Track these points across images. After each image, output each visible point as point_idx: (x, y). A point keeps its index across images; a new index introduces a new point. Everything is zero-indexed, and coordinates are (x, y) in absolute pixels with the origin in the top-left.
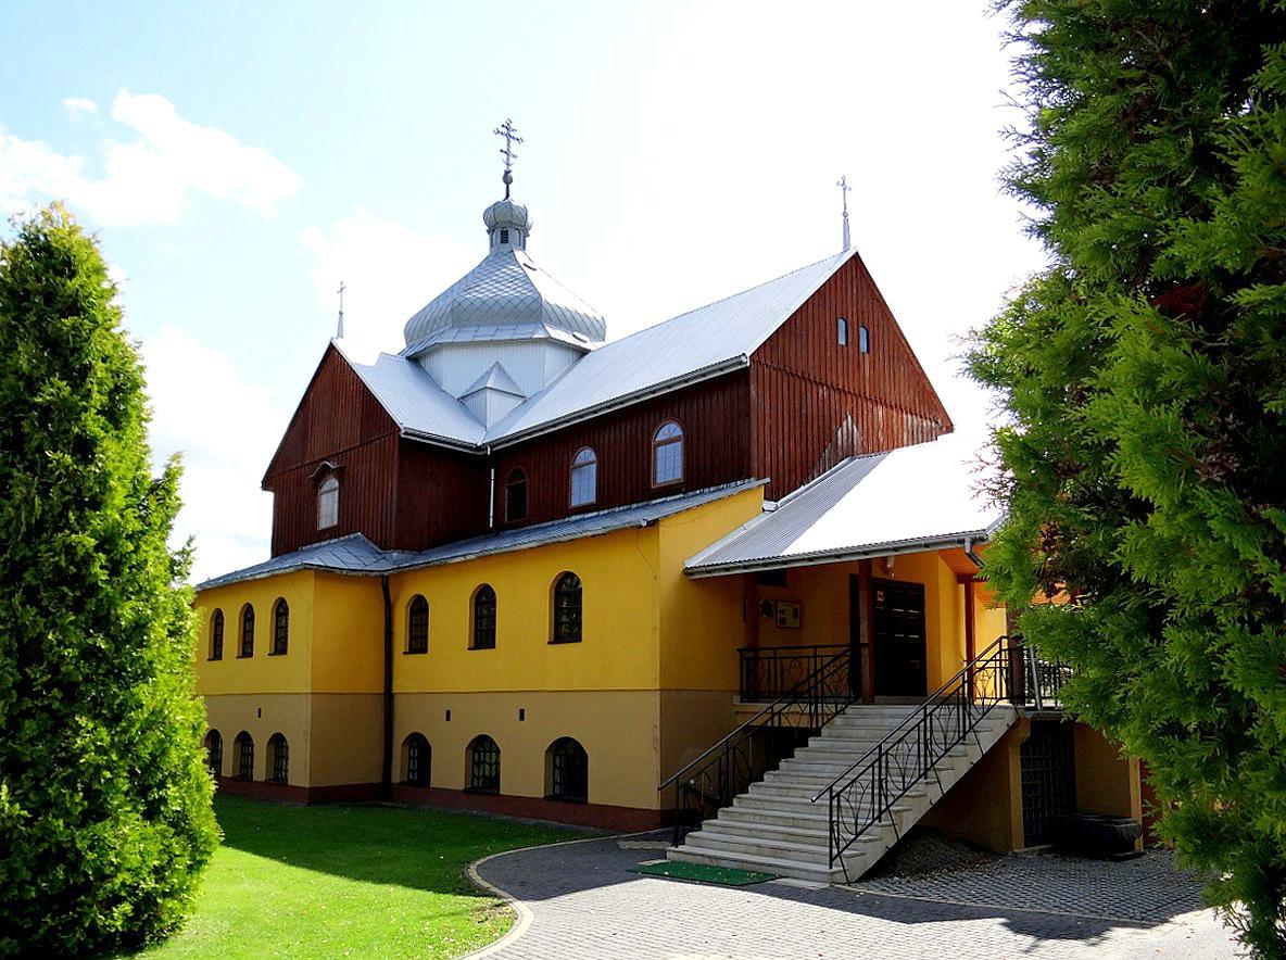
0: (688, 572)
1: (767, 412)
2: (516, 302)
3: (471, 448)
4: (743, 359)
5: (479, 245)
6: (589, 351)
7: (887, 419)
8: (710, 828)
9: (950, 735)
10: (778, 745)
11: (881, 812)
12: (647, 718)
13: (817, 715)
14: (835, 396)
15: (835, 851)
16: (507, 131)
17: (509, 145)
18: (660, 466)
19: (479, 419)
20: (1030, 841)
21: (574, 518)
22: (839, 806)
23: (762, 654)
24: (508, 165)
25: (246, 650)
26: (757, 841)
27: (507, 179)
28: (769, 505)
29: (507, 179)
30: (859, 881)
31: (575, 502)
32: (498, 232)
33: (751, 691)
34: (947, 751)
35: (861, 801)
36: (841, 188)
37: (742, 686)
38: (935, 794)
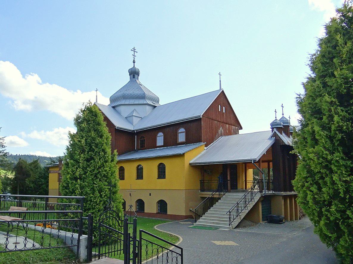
0: (190, 164)
1: (205, 127)
2: (139, 94)
3: (131, 131)
4: (201, 116)
5: (126, 78)
6: (157, 106)
7: (229, 127)
8: (202, 219)
9: (249, 199)
10: (211, 202)
11: (238, 215)
12: (183, 195)
13: (220, 195)
14: (218, 123)
15: (230, 223)
16: (134, 50)
17: (134, 54)
18: (179, 138)
19: (132, 123)
20: (263, 220)
21: (158, 148)
22: (231, 214)
23: (205, 181)
24: (134, 58)
25: (291, 220)
26: (213, 221)
27: (134, 62)
28: (206, 148)
29: (134, 62)
30: (235, 228)
31: (158, 145)
32: (132, 75)
33: (202, 190)
34: (249, 203)
35: (234, 213)
36: (219, 75)
37: (201, 188)
38: (247, 211)
